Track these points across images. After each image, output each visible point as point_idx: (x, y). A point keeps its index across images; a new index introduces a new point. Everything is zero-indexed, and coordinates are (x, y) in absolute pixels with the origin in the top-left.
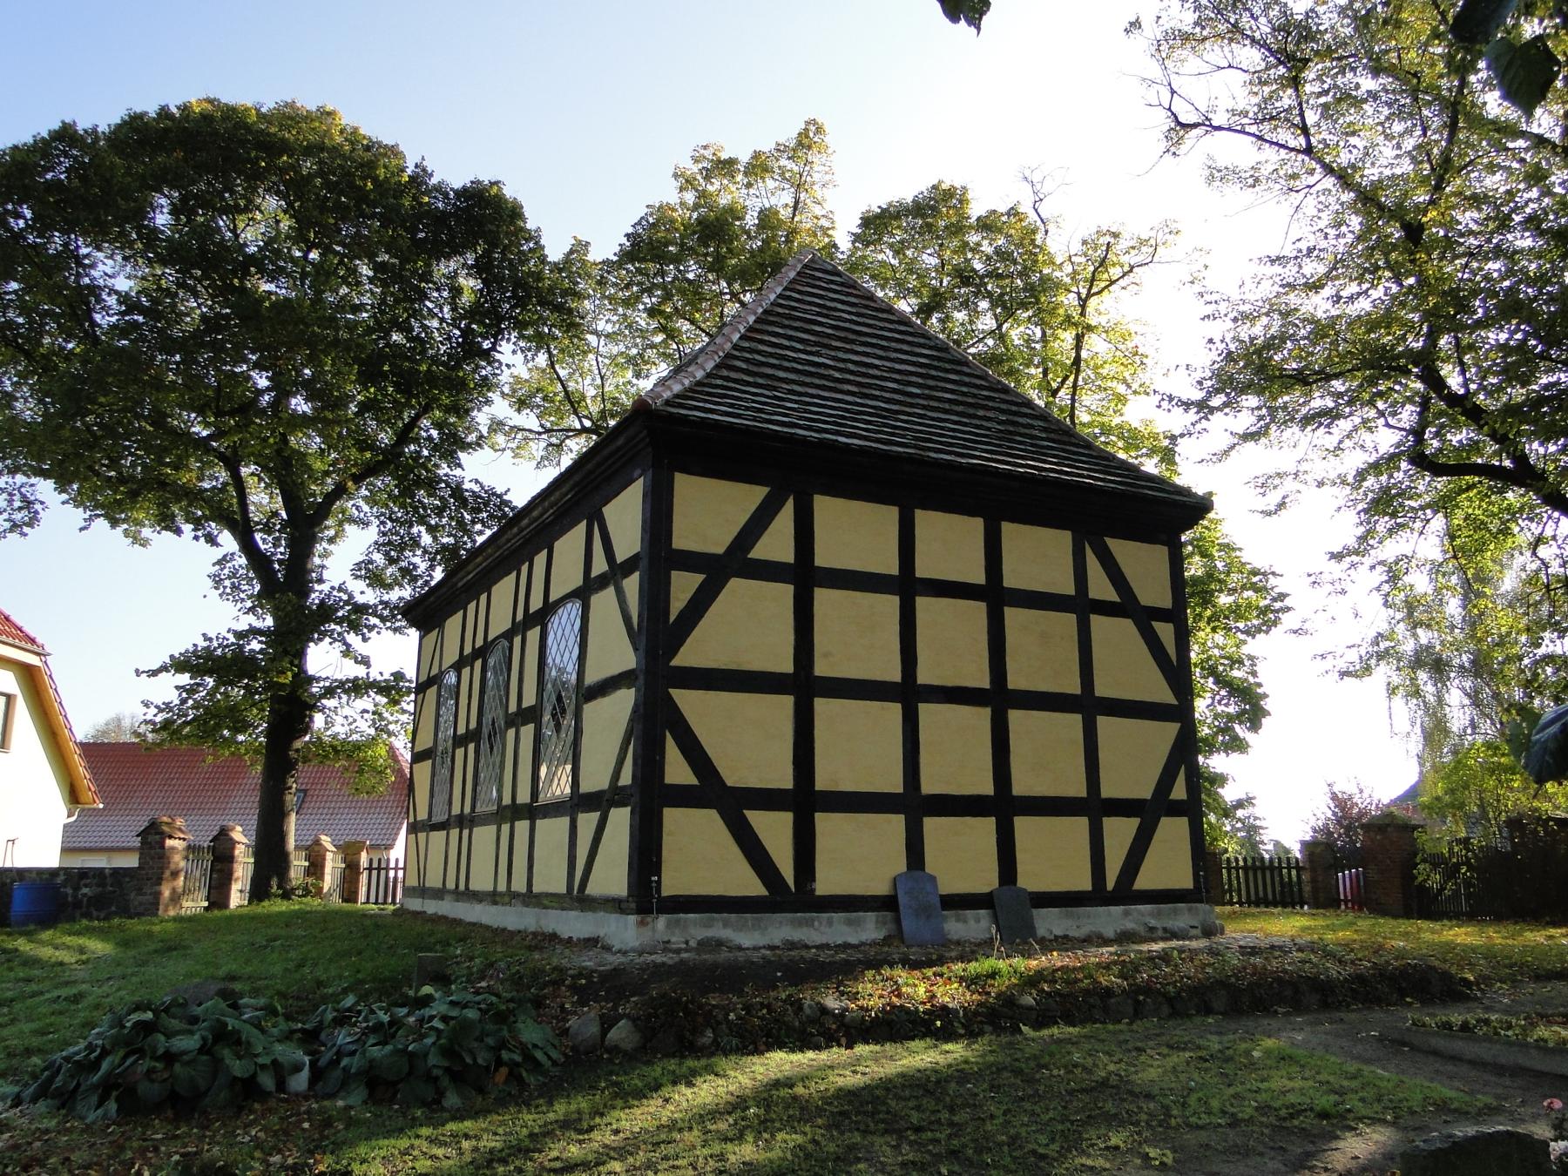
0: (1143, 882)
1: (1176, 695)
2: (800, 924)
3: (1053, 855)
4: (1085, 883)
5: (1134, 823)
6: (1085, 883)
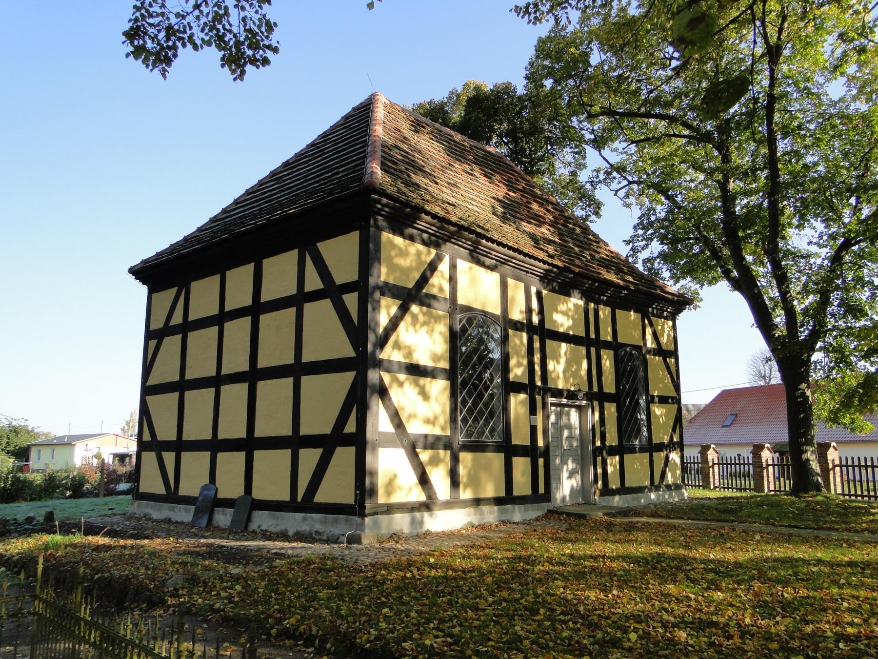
0: (322, 496)
1: (355, 349)
2: (172, 510)
3: (272, 475)
4: (286, 497)
5: (319, 452)
6: (286, 497)
